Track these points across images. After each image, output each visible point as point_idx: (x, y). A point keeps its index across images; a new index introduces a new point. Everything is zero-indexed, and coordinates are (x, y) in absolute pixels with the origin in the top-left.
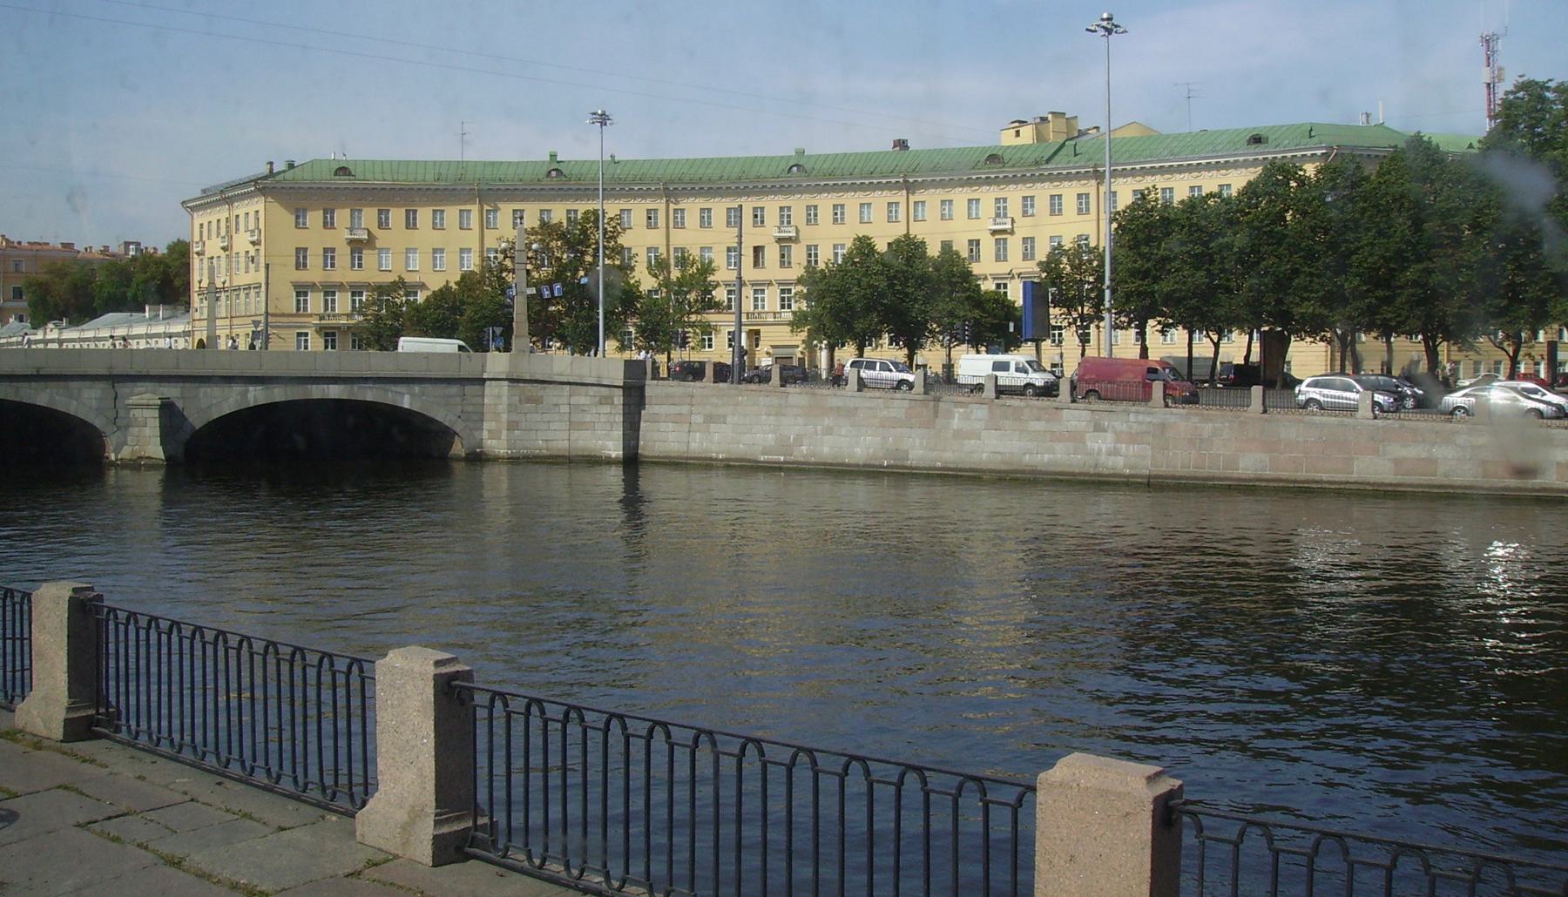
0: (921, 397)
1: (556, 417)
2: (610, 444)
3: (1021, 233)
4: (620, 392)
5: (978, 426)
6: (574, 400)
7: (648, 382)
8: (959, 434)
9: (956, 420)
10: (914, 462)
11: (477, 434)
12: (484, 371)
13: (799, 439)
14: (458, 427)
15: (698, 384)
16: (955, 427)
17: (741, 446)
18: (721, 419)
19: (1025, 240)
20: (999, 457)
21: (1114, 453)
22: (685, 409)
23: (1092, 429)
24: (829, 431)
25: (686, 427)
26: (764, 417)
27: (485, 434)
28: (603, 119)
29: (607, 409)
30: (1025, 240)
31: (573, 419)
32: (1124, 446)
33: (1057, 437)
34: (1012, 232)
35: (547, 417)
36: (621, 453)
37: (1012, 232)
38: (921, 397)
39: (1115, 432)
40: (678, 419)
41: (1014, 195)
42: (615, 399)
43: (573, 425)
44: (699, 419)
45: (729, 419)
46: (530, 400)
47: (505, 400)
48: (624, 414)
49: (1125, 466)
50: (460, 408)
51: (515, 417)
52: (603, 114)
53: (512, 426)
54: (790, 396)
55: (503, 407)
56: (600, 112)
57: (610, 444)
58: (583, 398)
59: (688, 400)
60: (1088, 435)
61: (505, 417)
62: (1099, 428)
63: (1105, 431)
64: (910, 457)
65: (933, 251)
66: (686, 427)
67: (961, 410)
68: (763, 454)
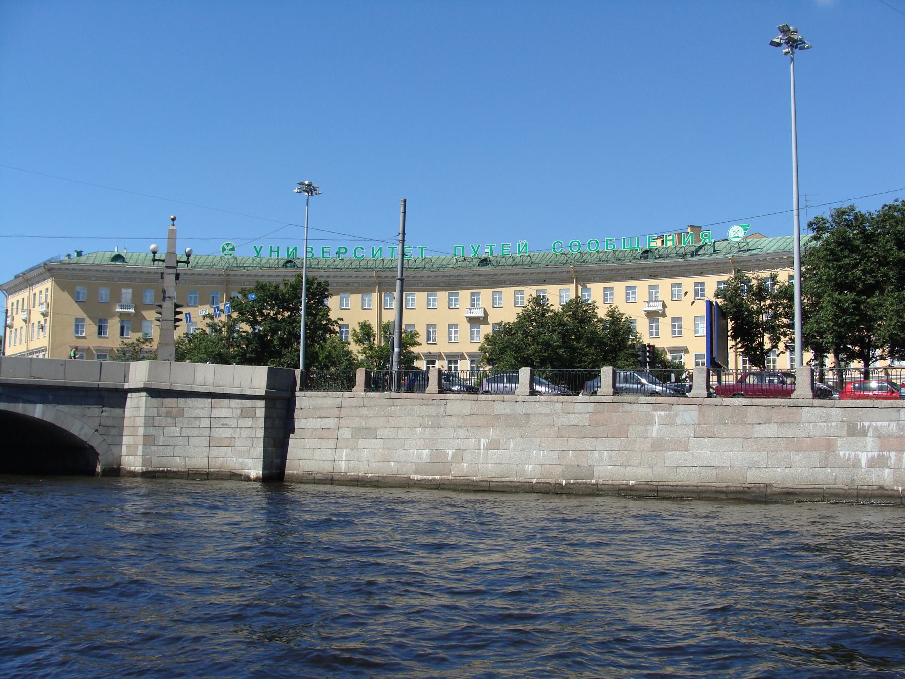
0: (610, 399)
1: (195, 432)
2: (250, 462)
3: (670, 313)
4: (262, 404)
5: (684, 432)
6: (216, 413)
7: (297, 393)
8: (658, 445)
9: (656, 426)
10: (601, 482)
11: (114, 449)
12: (125, 378)
13: (459, 453)
14: (95, 441)
15: (347, 394)
16: (654, 434)
17: (392, 464)
18: (370, 433)
19: (674, 320)
20: (714, 472)
21: (876, 463)
22: (331, 423)
23: (845, 433)
24: (494, 445)
25: (332, 443)
26: (419, 430)
27: (124, 449)
28: (310, 189)
29: (248, 422)
30: (674, 320)
31: (213, 434)
32: (893, 454)
33: (794, 445)
34: (664, 315)
35: (186, 432)
36: (261, 472)
37: (664, 315)
38: (610, 399)
39: (880, 436)
40: (323, 434)
41: (664, 285)
42: (258, 411)
43: (212, 442)
44: (346, 433)
45: (380, 433)
46: (168, 415)
47: (142, 412)
48: (265, 428)
49: (896, 482)
50: (97, 421)
51: (152, 431)
52: (310, 185)
53: (149, 440)
54: (449, 403)
55: (140, 421)
56: (306, 182)
57: (250, 462)
58: (225, 410)
59: (337, 411)
60: (839, 441)
61: (141, 431)
62: (854, 431)
63: (864, 433)
64: (596, 474)
65: (602, 313)
66: (332, 443)
67: (662, 413)
68: (416, 473)
